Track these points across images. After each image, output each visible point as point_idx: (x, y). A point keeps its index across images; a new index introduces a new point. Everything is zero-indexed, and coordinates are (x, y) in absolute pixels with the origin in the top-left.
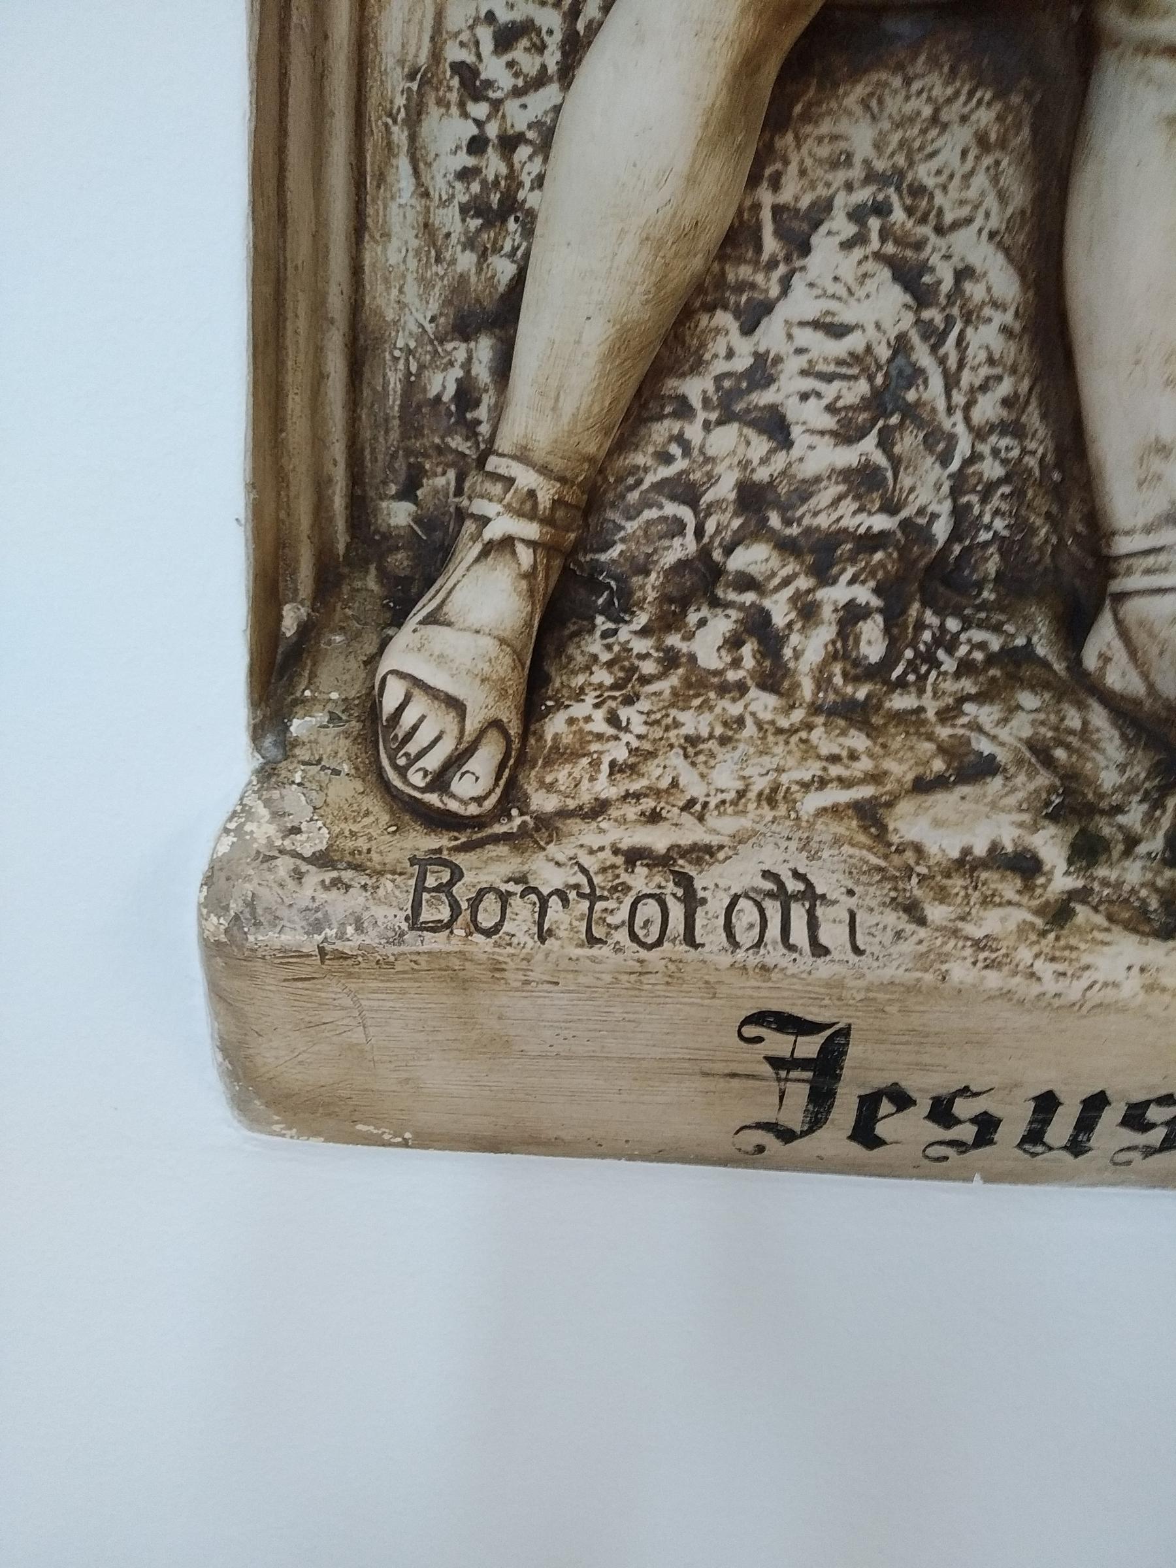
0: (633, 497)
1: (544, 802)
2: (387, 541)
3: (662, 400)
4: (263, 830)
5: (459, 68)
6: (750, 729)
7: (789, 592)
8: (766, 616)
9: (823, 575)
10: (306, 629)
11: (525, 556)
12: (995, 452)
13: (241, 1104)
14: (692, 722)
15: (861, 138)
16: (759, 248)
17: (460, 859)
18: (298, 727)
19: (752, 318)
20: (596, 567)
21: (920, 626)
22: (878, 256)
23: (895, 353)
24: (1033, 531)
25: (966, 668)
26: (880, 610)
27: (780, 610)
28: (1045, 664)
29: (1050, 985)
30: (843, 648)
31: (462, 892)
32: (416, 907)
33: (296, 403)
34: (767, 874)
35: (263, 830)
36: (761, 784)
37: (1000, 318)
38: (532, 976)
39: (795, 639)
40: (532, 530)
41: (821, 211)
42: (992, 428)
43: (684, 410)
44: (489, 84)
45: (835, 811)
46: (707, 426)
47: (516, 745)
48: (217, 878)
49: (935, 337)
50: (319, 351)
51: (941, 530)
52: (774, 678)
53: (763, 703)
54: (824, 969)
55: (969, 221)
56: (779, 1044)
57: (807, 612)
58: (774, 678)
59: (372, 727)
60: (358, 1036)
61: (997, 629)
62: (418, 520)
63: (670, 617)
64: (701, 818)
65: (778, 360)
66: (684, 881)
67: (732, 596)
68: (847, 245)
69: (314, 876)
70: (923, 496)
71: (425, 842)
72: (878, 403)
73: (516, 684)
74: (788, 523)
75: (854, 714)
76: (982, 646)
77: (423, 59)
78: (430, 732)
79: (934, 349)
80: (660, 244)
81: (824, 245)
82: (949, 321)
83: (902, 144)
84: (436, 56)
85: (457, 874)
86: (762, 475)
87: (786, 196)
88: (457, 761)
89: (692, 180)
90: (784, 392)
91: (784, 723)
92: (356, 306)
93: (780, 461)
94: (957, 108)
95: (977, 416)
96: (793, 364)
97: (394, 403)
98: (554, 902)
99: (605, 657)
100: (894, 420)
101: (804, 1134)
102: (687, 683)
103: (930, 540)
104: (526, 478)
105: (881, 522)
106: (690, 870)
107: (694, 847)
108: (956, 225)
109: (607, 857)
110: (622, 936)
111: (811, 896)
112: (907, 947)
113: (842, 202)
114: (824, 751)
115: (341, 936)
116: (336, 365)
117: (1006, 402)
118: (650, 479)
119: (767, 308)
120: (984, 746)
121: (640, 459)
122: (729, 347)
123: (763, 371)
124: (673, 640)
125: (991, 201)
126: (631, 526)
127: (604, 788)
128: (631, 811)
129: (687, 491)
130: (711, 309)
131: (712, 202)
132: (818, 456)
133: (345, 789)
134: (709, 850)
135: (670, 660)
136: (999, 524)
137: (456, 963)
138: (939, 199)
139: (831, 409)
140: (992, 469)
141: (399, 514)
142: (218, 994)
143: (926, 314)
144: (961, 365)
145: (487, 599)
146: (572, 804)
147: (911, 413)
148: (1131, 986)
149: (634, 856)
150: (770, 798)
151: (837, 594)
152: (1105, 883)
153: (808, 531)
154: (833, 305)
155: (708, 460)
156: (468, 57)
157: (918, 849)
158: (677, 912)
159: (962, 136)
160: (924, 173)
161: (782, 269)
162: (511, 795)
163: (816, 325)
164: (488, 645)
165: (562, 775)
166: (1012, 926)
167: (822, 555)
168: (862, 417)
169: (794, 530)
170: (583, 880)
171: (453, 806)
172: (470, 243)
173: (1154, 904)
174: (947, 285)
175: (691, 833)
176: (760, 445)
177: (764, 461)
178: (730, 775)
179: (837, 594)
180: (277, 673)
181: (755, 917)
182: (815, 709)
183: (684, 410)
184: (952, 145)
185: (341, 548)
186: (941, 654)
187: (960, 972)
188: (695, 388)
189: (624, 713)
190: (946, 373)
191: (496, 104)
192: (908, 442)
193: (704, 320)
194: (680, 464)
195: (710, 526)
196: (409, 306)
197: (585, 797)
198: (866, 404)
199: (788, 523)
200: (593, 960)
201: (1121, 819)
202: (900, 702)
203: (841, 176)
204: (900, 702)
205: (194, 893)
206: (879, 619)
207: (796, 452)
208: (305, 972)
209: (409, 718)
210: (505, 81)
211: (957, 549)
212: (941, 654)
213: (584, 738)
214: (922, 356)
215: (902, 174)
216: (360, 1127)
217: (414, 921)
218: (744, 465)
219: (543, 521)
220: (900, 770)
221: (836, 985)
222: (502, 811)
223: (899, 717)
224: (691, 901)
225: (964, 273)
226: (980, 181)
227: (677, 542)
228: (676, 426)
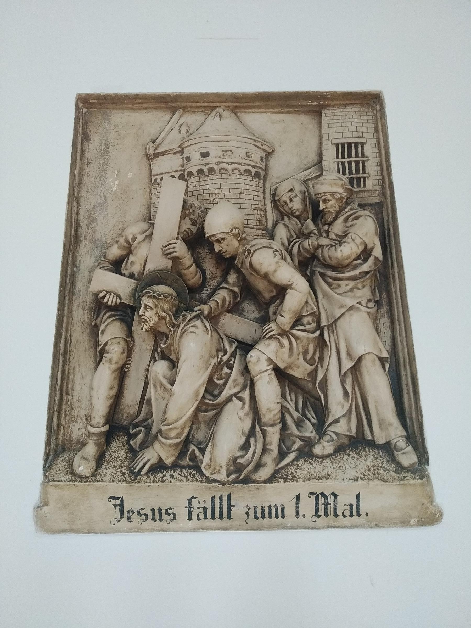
56: (114, 502)
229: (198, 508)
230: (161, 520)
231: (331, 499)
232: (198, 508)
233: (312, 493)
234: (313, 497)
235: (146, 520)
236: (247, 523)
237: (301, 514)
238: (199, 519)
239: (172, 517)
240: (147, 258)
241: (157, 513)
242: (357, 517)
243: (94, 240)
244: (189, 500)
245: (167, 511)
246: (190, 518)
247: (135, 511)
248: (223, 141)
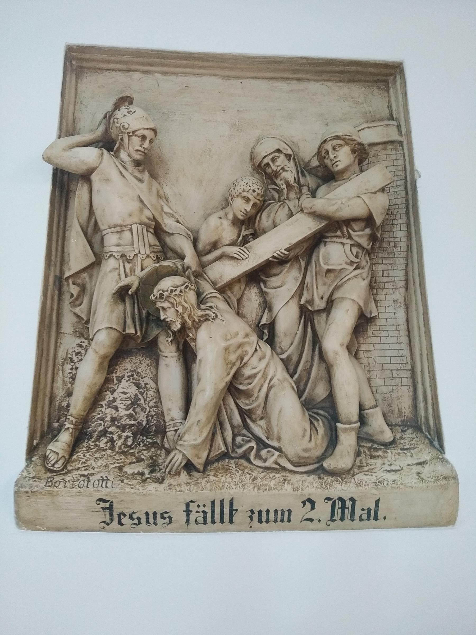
0: (94, 420)
1: (69, 468)
2: (54, 429)
3: (99, 405)
4: (25, 474)
5: (70, 358)
6: (106, 456)
7: (117, 434)
8: (113, 438)
9: (123, 432)
10: (38, 444)
11: (71, 430)
12: (153, 410)
13: (18, 524)
14: (96, 455)
15: (129, 366)
16: (114, 382)
17: (54, 477)
18: (33, 459)
19: (113, 392)
20: (87, 432)
21: (139, 439)
22: (132, 382)
23: (135, 396)
24: (161, 422)
25: (145, 445)
26: (132, 437)
27: (115, 437)
28: (158, 444)
29: (141, 491)
30: (125, 444)
31: (54, 481)
32: (46, 484)
33: (39, 409)
34: (101, 477)
35: (25, 474)
36: (105, 464)
37: (152, 390)
38: (63, 494)
39: (117, 442)
40: (72, 426)
41: (123, 376)
42: (153, 407)
43: (102, 406)
44: (74, 360)
45: (115, 467)
46: (106, 409)
47: (67, 460)
48: (17, 481)
49: (142, 394)
50: (44, 400)
51: (144, 423)
52: (112, 448)
53: (109, 452)
54: (107, 490)
55: (147, 376)
56: (103, 505)
57: (120, 437)
58: (112, 448)
59: (45, 458)
60: (36, 507)
61: (152, 439)
62: (59, 426)
63: (98, 440)
64: (94, 469)
65: (117, 398)
66: (88, 478)
67: (108, 435)
68: (127, 381)
69: (32, 480)
70: (141, 418)
71: (49, 475)
72: (133, 404)
73: (68, 450)
74: (118, 423)
75: (124, 453)
76: (148, 442)
77: (65, 357)
78: (53, 458)
79: (142, 395)
80: (90, 386)
81: (123, 381)
82: (144, 391)
83: (135, 366)
84: (67, 356)
85: (53, 479)
86: (114, 416)
87: (117, 375)
88: (56, 462)
89: (94, 378)
90: (117, 403)
91: (112, 455)
92: (52, 393)
93: (117, 414)
94: (144, 361)
95: (150, 405)
96: (119, 399)
97: (57, 407)
98: (68, 482)
99: (86, 446)
100: (136, 406)
101: (111, 523)
102: (98, 449)
103: (143, 425)
104: (71, 418)
105: (133, 422)
106: (90, 477)
107: (91, 473)
108: (145, 377)
109: (78, 476)
110: (77, 487)
111: (107, 480)
112: (120, 486)
113: (126, 375)
114: (116, 459)
115: (34, 489)
116: (47, 402)
117: (155, 403)
118: (96, 417)
119: (115, 391)
120: (143, 457)
121: (95, 414)
122: (109, 396)
123: (114, 400)
124: (97, 443)
125: (150, 373)
126: (93, 425)
127: (80, 466)
128: (83, 469)
129: (102, 419)
130: (106, 391)
131: (100, 379)
132: (123, 413)
133: (38, 468)
134: (94, 474)
135: (96, 446)
136: (155, 422)
137: (51, 492)
138: (142, 374)
139: (125, 405)
140: (153, 413)
141: (56, 425)
142: (15, 498)
143: (140, 390)
144: (147, 397)
145: (65, 437)
146: (74, 468)
147: (139, 405)
148: (153, 491)
149: (81, 475)
150: (105, 466)
151: (125, 434)
152: (154, 476)
153: (122, 424)
154: (125, 390)
155: (106, 414)
156: (71, 356)
157: (126, 472)
158: (86, 483)
159: (145, 365)
160: (139, 370)
161: (117, 385)
162: (65, 467)
163: (122, 393)
164: (64, 444)
165: (73, 464)
166: (136, 482)
167: (123, 428)
168: (130, 406)
169: (119, 424)
170: (73, 479)
171: (55, 469)
172: (70, 383)
173: (160, 479)
174: (143, 386)
175: (92, 471)
176: (114, 411)
177: (115, 414)
178: (97, 462)
179: (125, 434)
180: (31, 450)
181: (98, 483)
182: (118, 452)
183: (102, 406)
184: (143, 366)
185: (45, 431)
186: (141, 443)
187: (127, 490)
188: (104, 403)
189: (86, 454)
190: (144, 399)
191: (75, 363)
192: (138, 410)
193: (105, 393)
194: (101, 415)
195: (106, 424)
196: (60, 392)
197: (76, 467)
198: (130, 404)
199: (118, 423)
200: (73, 491)
201: (160, 467)
202: (132, 451)
203: (126, 371)
204: (132, 451)
205: (14, 484)
206: (132, 438)
207: (119, 412)
208: (28, 495)
209: (50, 456)
210: (76, 360)
211: (148, 426)
212: (141, 443)
213: (79, 458)
214: (140, 396)
215: (135, 370)
216: (37, 527)
217: (46, 486)
218: (111, 414)
219: (74, 425)
220: (128, 461)
221: (109, 493)
222: (63, 470)
223: (131, 453)
224: (89, 481)
225: (146, 384)
226: (148, 371)
227: (100, 427)
228: (101, 409)
229: (197, 512)
231: (348, 504)
232: (197, 512)
233: (328, 499)
236: (251, 527)
237: (380, 516)
239: (136, 521)
241: (151, 517)
244: (188, 505)
245: (162, 514)
246: (188, 521)
247: (127, 512)
248: (260, 78)
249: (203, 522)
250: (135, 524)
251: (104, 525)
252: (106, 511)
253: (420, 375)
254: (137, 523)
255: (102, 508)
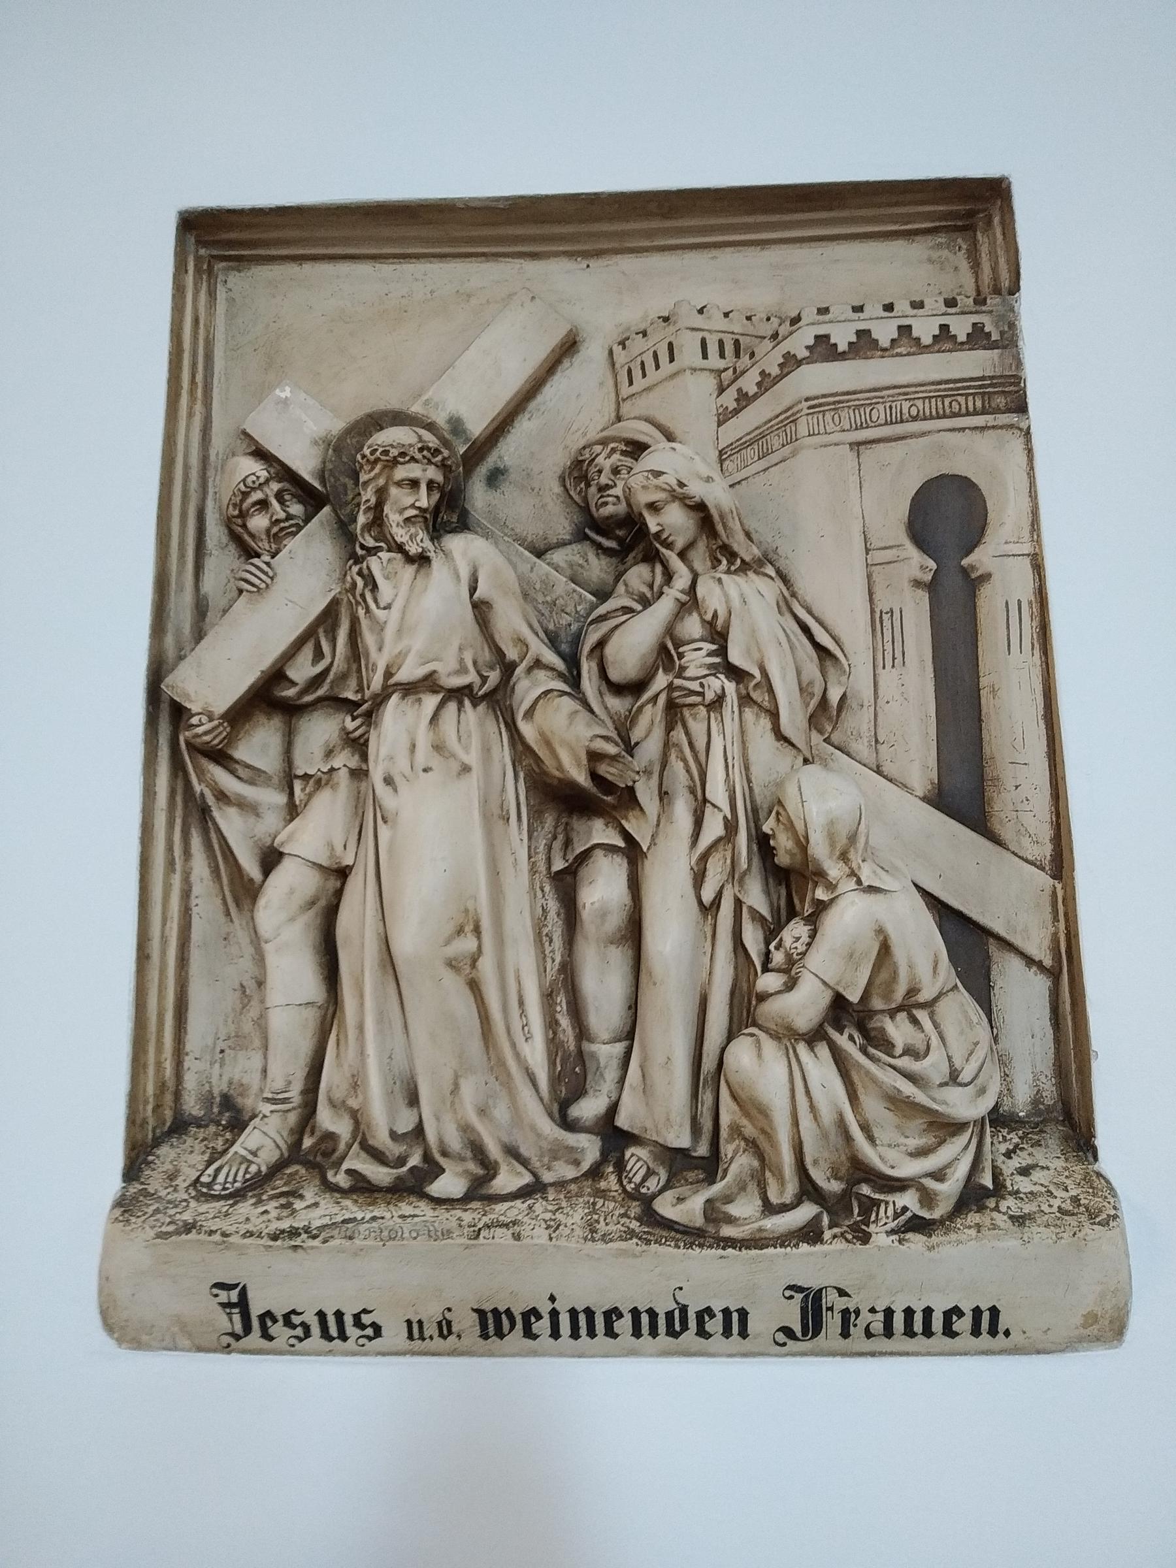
56: (223, 1296)
230: (343, 1337)
234: (799, 1297)
235: (246, 1336)
237: (1001, 1328)
238: (869, 1334)
239: (369, 1331)
240: (916, 886)
241: (918, 1319)
242: (552, 1340)
243: (360, 552)
245: (357, 1318)
247: (279, 1313)
249: (882, 1331)
250: (295, 1337)
251: (227, 1339)
252: (234, 1311)
253: (1013, 952)
254: (302, 1335)
255: (224, 1305)
